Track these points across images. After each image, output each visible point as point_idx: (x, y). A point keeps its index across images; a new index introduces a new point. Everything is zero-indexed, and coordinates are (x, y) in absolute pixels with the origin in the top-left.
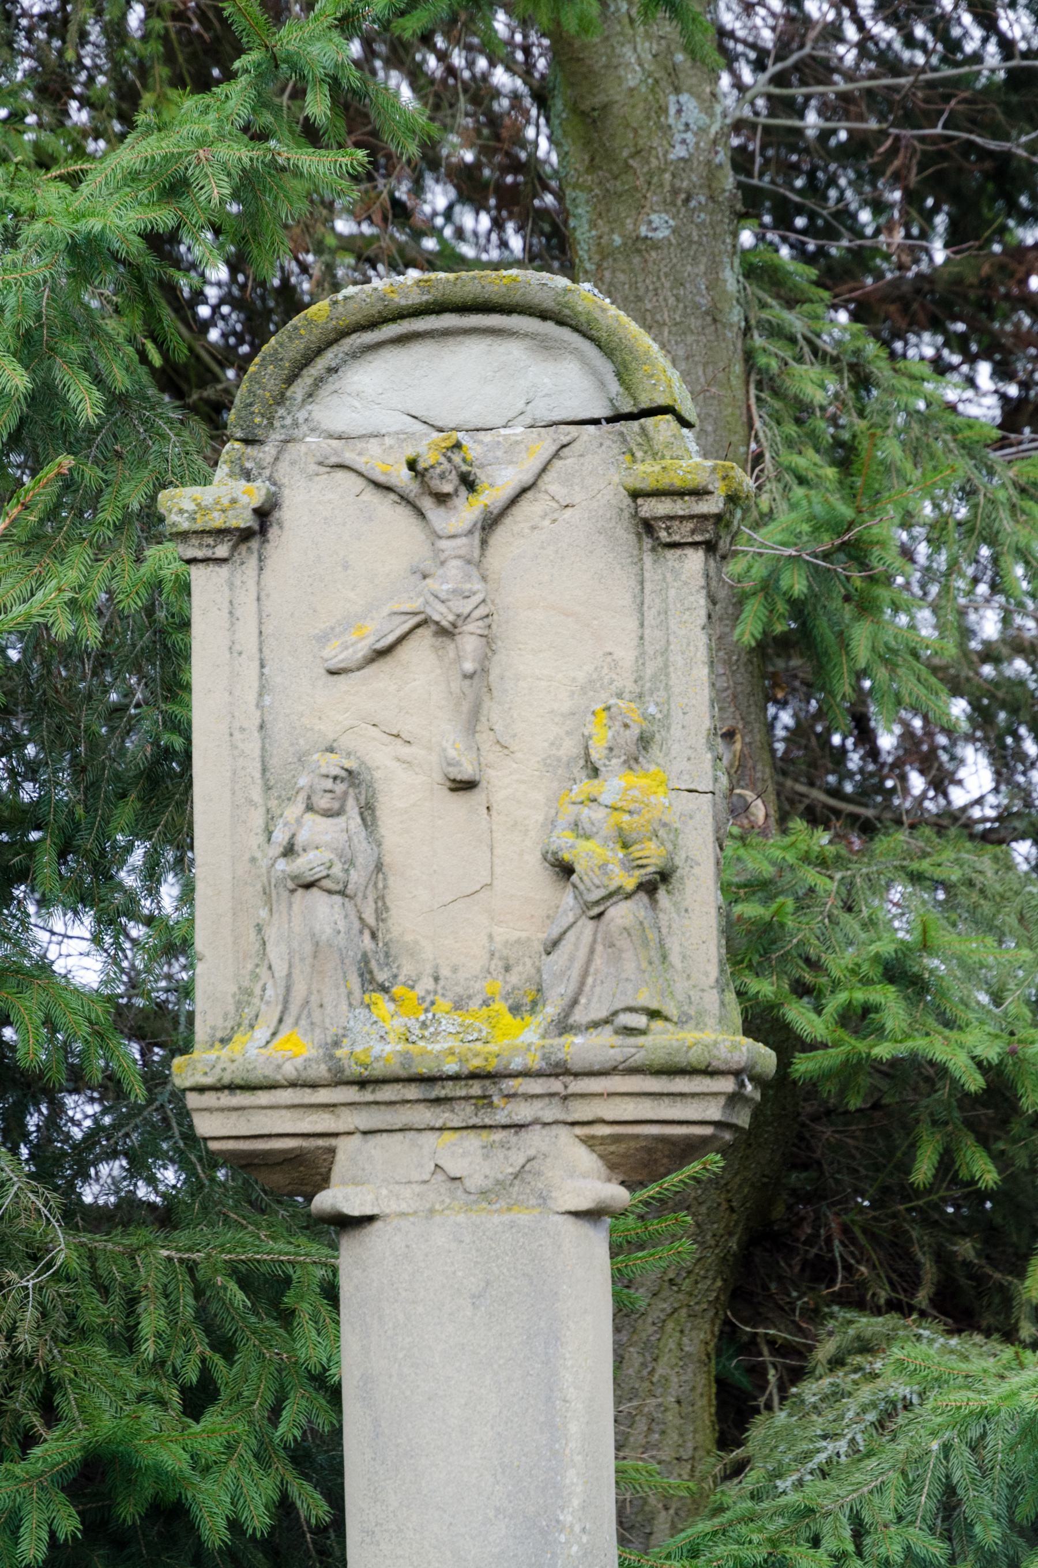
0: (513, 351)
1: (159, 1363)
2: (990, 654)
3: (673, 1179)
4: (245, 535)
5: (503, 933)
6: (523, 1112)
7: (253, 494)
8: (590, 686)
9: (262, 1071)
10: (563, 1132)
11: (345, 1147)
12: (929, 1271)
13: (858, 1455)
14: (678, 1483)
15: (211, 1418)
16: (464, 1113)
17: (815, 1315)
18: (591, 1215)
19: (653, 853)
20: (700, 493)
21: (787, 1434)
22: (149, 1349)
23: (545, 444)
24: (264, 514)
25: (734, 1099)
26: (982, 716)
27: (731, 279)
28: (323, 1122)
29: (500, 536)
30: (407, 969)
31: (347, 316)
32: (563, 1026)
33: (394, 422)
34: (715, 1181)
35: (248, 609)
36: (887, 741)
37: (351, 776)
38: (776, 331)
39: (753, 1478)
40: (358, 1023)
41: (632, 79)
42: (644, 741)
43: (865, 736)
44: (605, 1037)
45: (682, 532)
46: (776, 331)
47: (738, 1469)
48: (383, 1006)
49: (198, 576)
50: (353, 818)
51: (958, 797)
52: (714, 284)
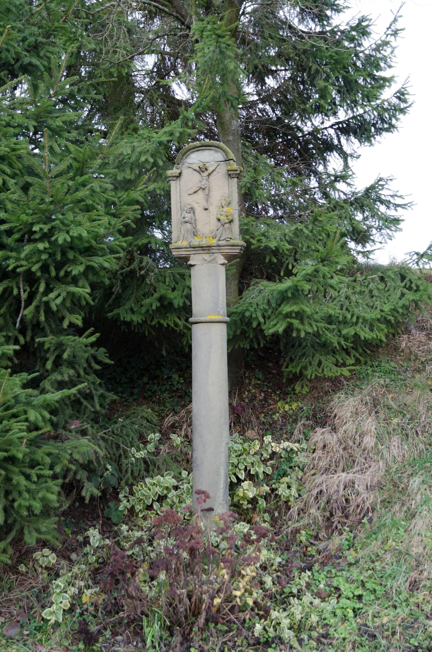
0: (212, 152)
1: (168, 285)
2: (273, 196)
3: (233, 262)
4: (178, 177)
5: (211, 228)
6: (214, 251)
7: (178, 171)
8: (222, 196)
9: (181, 246)
10: (219, 254)
11: (192, 256)
12: (265, 274)
13: (256, 296)
14: (234, 300)
15: (175, 292)
16: (206, 252)
17: (251, 279)
18: (223, 264)
19: (230, 218)
20: (236, 170)
21: (247, 294)
22: (167, 283)
23: (216, 164)
24: (180, 174)
25: (241, 249)
26: (272, 204)
27: (240, 145)
28: (189, 253)
29: (211, 177)
30: (199, 233)
31: (190, 147)
32: (219, 240)
33: (196, 161)
34: (238, 262)
35: (178, 186)
36: (260, 207)
37: (192, 208)
38: (246, 152)
39: (243, 299)
40: (193, 240)
41: (227, 118)
42: (229, 203)
43: (257, 207)
44: (224, 242)
45: (234, 176)
46: (246, 152)
47: (241, 298)
48: (196, 238)
49: (171, 182)
50: (192, 214)
51: (269, 215)
52: (238, 146)
